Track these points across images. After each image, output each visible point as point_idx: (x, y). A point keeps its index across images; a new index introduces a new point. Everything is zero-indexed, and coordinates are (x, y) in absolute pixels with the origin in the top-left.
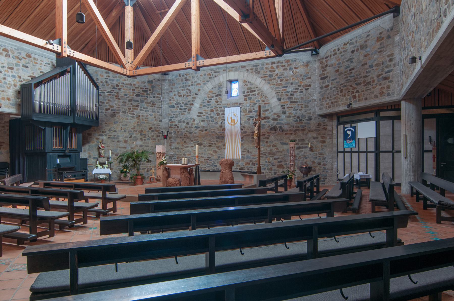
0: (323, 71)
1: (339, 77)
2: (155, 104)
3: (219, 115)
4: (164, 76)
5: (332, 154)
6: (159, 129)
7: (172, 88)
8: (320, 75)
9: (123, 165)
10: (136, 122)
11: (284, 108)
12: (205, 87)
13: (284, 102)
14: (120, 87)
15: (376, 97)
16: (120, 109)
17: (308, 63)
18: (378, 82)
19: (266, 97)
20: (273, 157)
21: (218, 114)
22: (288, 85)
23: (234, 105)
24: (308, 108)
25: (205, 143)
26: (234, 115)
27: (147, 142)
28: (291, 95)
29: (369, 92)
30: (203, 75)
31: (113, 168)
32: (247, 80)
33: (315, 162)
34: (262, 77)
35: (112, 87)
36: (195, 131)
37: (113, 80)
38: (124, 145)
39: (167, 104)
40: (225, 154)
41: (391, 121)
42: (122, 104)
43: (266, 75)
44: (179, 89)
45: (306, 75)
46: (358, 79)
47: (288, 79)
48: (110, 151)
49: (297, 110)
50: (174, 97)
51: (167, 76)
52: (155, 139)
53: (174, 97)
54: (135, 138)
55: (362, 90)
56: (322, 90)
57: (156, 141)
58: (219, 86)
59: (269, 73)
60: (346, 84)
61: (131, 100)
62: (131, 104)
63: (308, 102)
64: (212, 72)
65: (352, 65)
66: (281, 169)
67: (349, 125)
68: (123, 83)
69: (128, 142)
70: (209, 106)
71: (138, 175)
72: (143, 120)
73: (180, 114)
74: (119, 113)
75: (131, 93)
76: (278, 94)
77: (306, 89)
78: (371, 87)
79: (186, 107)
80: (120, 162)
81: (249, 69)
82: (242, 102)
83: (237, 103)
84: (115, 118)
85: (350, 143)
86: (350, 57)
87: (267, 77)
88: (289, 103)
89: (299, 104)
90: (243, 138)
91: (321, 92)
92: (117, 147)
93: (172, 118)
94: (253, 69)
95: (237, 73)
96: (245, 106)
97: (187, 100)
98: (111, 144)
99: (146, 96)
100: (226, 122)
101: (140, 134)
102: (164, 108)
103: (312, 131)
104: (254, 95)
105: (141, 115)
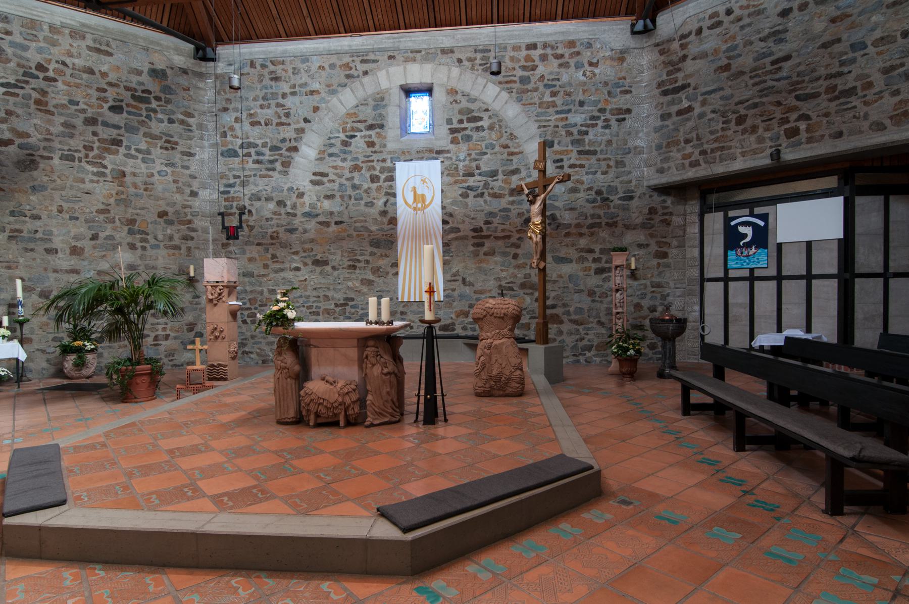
0: (669, 73)
1: (730, 83)
2: (176, 143)
3: (378, 182)
4: (203, 63)
5: (684, 285)
6: (189, 217)
7: (228, 100)
8: (659, 85)
9: (71, 326)
10: (114, 192)
11: (562, 167)
12: (334, 100)
13: (561, 153)
14: (51, 74)
15: (879, 127)
16: (52, 144)
17: (625, 52)
18: (886, 88)
19: (512, 137)
20: (532, 294)
21: (374, 179)
22: (571, 107)
23: (421, 155)
24: (623, 170)
25: (336, 258)
26: (423, 181)
27: (151, 256)
28: (580, 132)
29: (851, 115)
30: (327, 67)
31: (33, 337)
32: (459, 87)
33: (641, 307)
34: (500, 83)
35: (21, 71)
36: (306, 226)
37: (25, 48)
38: (72, 262)
39: (212, 146)
40: (397, 288)
41: (882, 197)
42: (61, 129)
43: (512, 78)
44: (252, 104)
45: (619, 83)
46: (804, 85)
47: (571, 92)
48: (19, 282)
49: (596, 172)
50: (237, 126)
51: (211, 64)
52: (177, 248)
53: (237, 126)
54: (109, 242)
55: (825, 111)
56: (669, 122)
57: (181, 254)
58: (375, 100)
59: (520, 73)
60: (757, 100)
61: (91, 121)
62: (95, 134)
63: (623, 154)
64: (353, 61)
65: (784, 48)
66: (555, 325)
67: (746, 211)
68: (64, 64)
69: (86, 255)
70: (346, 156)
71: (139, 363)
72: (135, 186)
73: (255, 175)
74: (52, 158)
75: (94, 100)
76: (545, 129)
77: (618, 120)
78: (855, 101)
79: (275, 155)
80: (59, 319)
81: (463, 58)
82: (443, 149)
83: (431, 151)
84: (35, 173)
85: (748, 256)
86: (777, 28)
87: (515, 82)
88: (574, 155)
89: (602, 157)
90: (448, 245)
91: (662, 127)
92: (46, 269)
93: (231, 186)
94: (475, 59)
95: (428, 67)
96: (454, 158)
97: (276, 136)
98: (21, 260)
99: (144, 114)
100: (399, 200)
101: (126, 228)
102: (202, 156)
103: (634, 229)
104: (478, 129)
105: (128, 170)
